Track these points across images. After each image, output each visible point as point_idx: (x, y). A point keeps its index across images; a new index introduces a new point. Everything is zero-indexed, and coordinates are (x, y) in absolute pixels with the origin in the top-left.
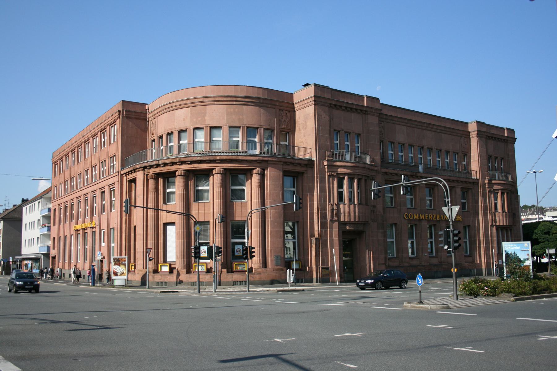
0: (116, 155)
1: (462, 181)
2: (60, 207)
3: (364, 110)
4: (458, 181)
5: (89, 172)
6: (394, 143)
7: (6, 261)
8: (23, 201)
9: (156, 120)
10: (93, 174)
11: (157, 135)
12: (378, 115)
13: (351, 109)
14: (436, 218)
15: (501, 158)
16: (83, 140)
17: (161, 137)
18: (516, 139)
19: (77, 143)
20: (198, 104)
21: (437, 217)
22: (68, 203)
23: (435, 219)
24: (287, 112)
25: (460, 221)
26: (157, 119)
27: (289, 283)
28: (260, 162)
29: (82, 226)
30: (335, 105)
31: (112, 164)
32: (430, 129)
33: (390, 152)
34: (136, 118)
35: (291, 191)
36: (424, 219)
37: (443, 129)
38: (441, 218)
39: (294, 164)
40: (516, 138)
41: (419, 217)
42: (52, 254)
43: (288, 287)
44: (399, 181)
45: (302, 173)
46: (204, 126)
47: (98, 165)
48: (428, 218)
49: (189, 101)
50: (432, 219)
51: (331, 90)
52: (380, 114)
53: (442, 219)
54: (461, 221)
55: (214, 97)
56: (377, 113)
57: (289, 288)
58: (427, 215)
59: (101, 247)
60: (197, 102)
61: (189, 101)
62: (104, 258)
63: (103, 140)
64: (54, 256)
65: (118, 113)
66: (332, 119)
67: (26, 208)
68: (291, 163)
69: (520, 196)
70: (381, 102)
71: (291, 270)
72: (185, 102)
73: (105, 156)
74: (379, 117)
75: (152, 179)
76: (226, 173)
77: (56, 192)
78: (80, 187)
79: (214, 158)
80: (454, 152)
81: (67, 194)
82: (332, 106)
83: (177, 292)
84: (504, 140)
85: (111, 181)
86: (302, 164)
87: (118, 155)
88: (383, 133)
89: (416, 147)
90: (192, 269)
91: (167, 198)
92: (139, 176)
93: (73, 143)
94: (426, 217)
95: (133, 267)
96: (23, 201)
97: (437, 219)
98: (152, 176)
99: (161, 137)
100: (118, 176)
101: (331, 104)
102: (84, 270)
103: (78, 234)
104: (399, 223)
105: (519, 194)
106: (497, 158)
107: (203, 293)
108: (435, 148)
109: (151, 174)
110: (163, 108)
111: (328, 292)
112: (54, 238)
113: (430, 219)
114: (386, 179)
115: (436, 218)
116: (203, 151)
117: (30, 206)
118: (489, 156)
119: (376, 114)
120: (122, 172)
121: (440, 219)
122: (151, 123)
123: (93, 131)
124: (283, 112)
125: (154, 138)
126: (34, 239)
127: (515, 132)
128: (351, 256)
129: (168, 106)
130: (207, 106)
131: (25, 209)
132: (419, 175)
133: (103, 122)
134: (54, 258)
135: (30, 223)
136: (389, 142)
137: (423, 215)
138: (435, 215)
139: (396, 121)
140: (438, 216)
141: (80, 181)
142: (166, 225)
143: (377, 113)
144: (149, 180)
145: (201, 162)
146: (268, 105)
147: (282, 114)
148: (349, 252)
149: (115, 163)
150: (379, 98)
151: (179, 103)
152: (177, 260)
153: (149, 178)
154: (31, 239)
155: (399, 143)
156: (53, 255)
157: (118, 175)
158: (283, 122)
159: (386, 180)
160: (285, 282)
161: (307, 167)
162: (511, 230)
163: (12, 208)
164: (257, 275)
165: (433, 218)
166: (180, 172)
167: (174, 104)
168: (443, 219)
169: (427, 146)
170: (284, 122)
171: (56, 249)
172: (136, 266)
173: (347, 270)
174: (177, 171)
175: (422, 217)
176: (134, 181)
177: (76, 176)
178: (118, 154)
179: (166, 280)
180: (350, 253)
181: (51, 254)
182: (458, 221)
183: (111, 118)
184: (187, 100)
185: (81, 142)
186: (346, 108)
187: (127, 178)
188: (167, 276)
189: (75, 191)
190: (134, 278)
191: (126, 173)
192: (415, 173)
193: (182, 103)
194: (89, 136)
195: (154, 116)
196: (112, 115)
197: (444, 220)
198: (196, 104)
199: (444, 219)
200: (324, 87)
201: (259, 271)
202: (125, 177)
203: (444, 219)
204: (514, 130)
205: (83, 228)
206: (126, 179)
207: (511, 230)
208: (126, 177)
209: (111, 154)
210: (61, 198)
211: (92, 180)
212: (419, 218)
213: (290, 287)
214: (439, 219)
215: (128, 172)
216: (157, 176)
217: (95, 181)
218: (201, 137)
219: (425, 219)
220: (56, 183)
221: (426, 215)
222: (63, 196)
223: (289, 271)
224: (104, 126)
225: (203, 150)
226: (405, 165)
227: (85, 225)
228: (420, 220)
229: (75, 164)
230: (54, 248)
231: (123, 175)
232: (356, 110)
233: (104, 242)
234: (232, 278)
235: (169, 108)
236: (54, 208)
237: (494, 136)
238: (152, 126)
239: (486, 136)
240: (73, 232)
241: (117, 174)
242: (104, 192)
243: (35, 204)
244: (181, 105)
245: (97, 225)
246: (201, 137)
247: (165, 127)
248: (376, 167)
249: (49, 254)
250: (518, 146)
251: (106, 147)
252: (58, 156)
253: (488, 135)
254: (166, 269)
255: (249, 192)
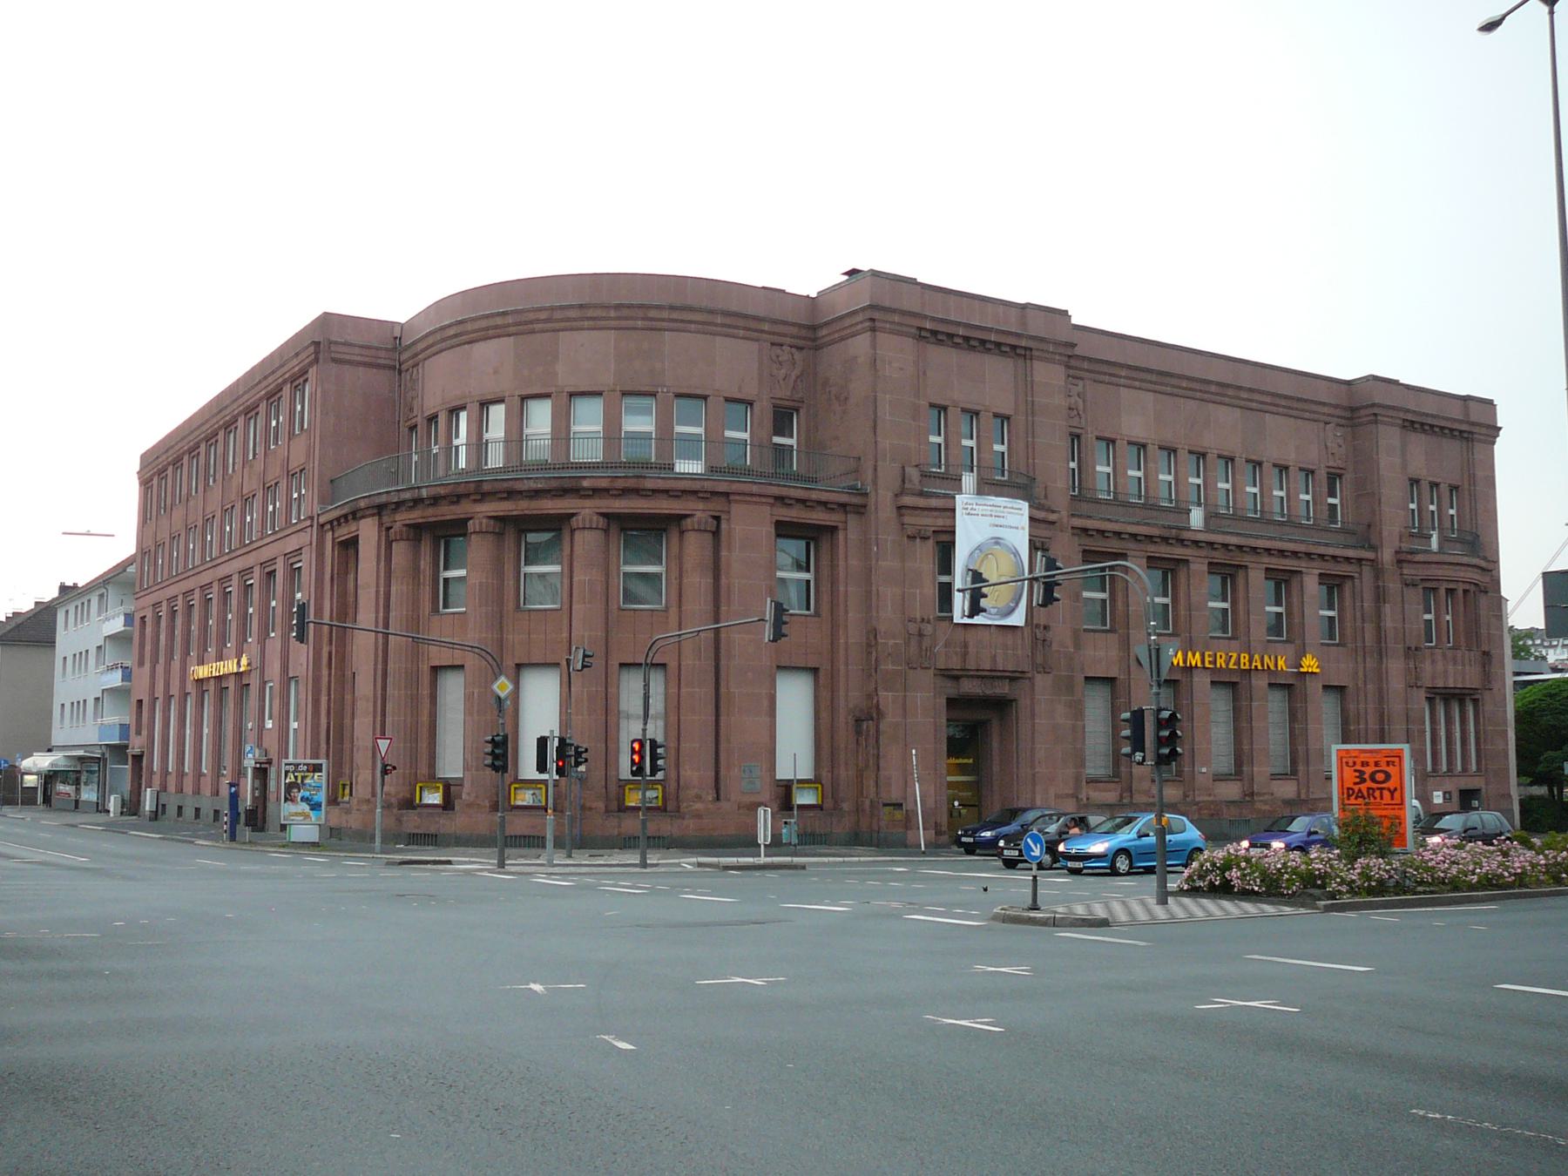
0: (307, 468)
1: (1322, 556)
2: (189, 601)
3: (1022, 347)
4: (1308, 555)
5: (237, 511)
6: (1113, 441)
7: (6, 765)
8: (64, 589)
9: (420, 371)
10: (267, 510)
11: (422, 411)
12: (1066, 359)
13: (983, 342)
14: (1238, 662)
15: (1450, 485)
16: (221, 423)
17: (433, 419)
18: (1500, 428)
19: (204, 428)
20: (535, 326)
21: (1242, 661)
22: (180, 601)
23: (1234, 664)
24: (794, 350)
25: (1312, 673)
26: (423, 367)
27: (762, 846)
28: (705, 496)
29: (214, 670)
30: (934, 333)
31: (295, 495)
32: (1227, 400)
33: (1102, 469)
34: (365, 364)
35: (798, 580)
36: (1199, 665)
37: (1268, 399)
38: (1254, 664)
39: (808, 504)
40: (1499, 425)
41: (1185, 661)
42: (133, 748)
43: (760, 856)
44: (1126, 554)
45: (833, 530)
46: (553, 389)
47: (260, 495)
48: (1215, 662)
49: (510, 320)
50: (1224, 666)
51: (922, 288)
52: (1070, 357)
53: (1256, 666)
54: (1315, 673)
55: (581, 306)
56: (1060, 354)
57: (763, 860)
58: (1210, 653)
59: (264, 732)
60: (531, 322)
61: (510, 320)
62: (270, 762)
63: (274, 423)
64: (139, 753)
65: (312, 349)
66: (925, 373)
67: (67, 612)
68: (798, 500)
69: (1507, 600)
70: (1074, 321)
71: (769, 809)
72: (499, 321)
73: (278, 471)
74: (1068, 367)
75: (402, 539)
76: (609, 525)
77: (191, 546)
78: (274, 529)
79: (574, 484)
80: (1301, 469)
81: (177, 575)
82: (923, 334)
83: (449, 862)
84: (1461, 432)
85: (292, 544)
86: (831, 503)
87: (311, 470)
88: (1081, 413)
89: (1183, 454)
90: (257, 798)
91: (443, 593)
92: (368, 531)
93: (195, 430)
94: (1207, 659)
95: (347, 791)
96: (64, 589)
97: (1242, 667)
98: (401, 531)
99: (433, 419)
100: (309, 530)
101: (920, 329)
102: (217, 795)
103: (203, 692)
104: (1122, 677)
105: (1503, 594)
106: (1437, 485)
107: (513, 869)
108: (1244, 456)
109: (397, 527)
110: (438, 336)
111: (875, 872)
112: (140, 702)
113: (1218, 665)
114: (1087, 548)
115: (1238, 662)
116: (549, 461)
117: (77, 607)
118: (1410, 479)
119: (1057, 357)
120: (322, 520)
121: (1250, 665)
122: (408, 377)
123: (246, 397)
124: (783, 351)
125: (414, 421)
126: (85, 701)
127: (1498, 407)
128: (972, 770)
129: (452, 332)
130: (561, 333)
131: (64, 613)
132: (1186, 535)
133: (273, 372)
134: (138, 759)
135: (75, 655)
136: (1098, 438)
137: (1198, 655)
138: (1235, 656)
139: (1120, 377)
140: (1245, 657)
141: (252, 519)
142: (436, 670)
143: (1060, 354)
144: (394, 544)
145: (536, 494)
146: (736, 331)
147: (778, 356)
148: (969, 758)
149: (303, 492)
150: (1067, 311)
151: (484, 323)
152: (466, 772)
153: (392, 537)
154: (78, 702)
155: (1130, 443)
156: (137, 751)
157: (312, 526)
158: (781, 382)
159: (1084, 551)
160: (750, 844)
161: (846, 513)
162: (1475, 701)
163: (32, 610)
164: (691, 821)
165: (1227, 664)
166: (477, 522)
167: (469, 327)
168: (1260, 667)
169: (1215, 452)
170: (784, 379)
171: (145, 732)
172: (354, 786)
173: (964, 811)
174: (471, 518)
175: (1194, 660)
176: (351, 545)
177: (200, 523)
178: (311, 465)
179: (432, 830)
180: (971, 761)
181: (130, 747)
182: (1308, 672)
183: (295, 361)
184: (504, 314)
185: (216, 426)
186: (967, 339)
187: (336, 535)
188: (437, 819)
189: (198, 566)
190: (347, 822)
191: (331, 522)
192: (1174, 531)
193: (491, 322)
194: (236, 412)
195: (415, 359)
196: (297, 355)
197: (1263, 670)
198: (531, 326)
199: (1263, 665)
200: (900, 281)
201: (697, 810)
202: (331, 533)
203: (1263, 665)
204: (1495, 403)
205: (218, 674)
206: (333, 539)
207: (1475, 701)
208: (333, 531)
209: (294, 464)
210: (177, 579)
211: (221, 546)
212: (1185, 661)
213: (765, 856)
214: (1247, 667)
215: (338, 519)
216: (417, 531)
217: (275, 533)
218: (540, 418)
219: (1204, 668)
220: (164, 535)
221: (1207, 653)
222: (182, 573)
223: (762, 811)
224: (276, 383)
225: (547, 461)
226: (1144, 506)
227: (222, 668)
228: (1189, 670)
229: (199, 491)
230: (139, 733)
231: (322, 526)
232: (998, 345)
233: (270, 718)
234: (619, 826)
235: (456, 336)
236: (142, 615)
237: (1430, 421)
238: (409, 385)
239: (1404, 420)
240: (190, 688)
241: (308, 523)
242: (271, 574)
243: (89, 601)
244: (487, 329)
245: (254, 666)
246: (540, 418)
247: (443, 391)
248: (1053, 512)
249: (126, 747)
250: (1503, 450)
251: (280, 443)
252: (154, 465)
253: (1410, 417)
254: (434, 798)
255: (675, 582)
